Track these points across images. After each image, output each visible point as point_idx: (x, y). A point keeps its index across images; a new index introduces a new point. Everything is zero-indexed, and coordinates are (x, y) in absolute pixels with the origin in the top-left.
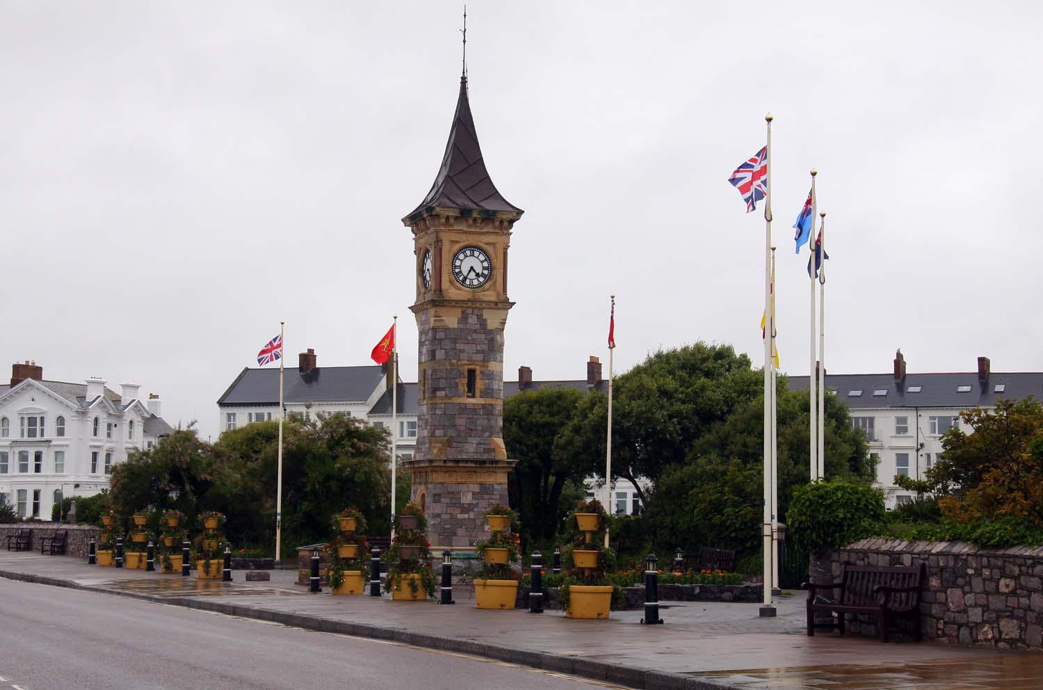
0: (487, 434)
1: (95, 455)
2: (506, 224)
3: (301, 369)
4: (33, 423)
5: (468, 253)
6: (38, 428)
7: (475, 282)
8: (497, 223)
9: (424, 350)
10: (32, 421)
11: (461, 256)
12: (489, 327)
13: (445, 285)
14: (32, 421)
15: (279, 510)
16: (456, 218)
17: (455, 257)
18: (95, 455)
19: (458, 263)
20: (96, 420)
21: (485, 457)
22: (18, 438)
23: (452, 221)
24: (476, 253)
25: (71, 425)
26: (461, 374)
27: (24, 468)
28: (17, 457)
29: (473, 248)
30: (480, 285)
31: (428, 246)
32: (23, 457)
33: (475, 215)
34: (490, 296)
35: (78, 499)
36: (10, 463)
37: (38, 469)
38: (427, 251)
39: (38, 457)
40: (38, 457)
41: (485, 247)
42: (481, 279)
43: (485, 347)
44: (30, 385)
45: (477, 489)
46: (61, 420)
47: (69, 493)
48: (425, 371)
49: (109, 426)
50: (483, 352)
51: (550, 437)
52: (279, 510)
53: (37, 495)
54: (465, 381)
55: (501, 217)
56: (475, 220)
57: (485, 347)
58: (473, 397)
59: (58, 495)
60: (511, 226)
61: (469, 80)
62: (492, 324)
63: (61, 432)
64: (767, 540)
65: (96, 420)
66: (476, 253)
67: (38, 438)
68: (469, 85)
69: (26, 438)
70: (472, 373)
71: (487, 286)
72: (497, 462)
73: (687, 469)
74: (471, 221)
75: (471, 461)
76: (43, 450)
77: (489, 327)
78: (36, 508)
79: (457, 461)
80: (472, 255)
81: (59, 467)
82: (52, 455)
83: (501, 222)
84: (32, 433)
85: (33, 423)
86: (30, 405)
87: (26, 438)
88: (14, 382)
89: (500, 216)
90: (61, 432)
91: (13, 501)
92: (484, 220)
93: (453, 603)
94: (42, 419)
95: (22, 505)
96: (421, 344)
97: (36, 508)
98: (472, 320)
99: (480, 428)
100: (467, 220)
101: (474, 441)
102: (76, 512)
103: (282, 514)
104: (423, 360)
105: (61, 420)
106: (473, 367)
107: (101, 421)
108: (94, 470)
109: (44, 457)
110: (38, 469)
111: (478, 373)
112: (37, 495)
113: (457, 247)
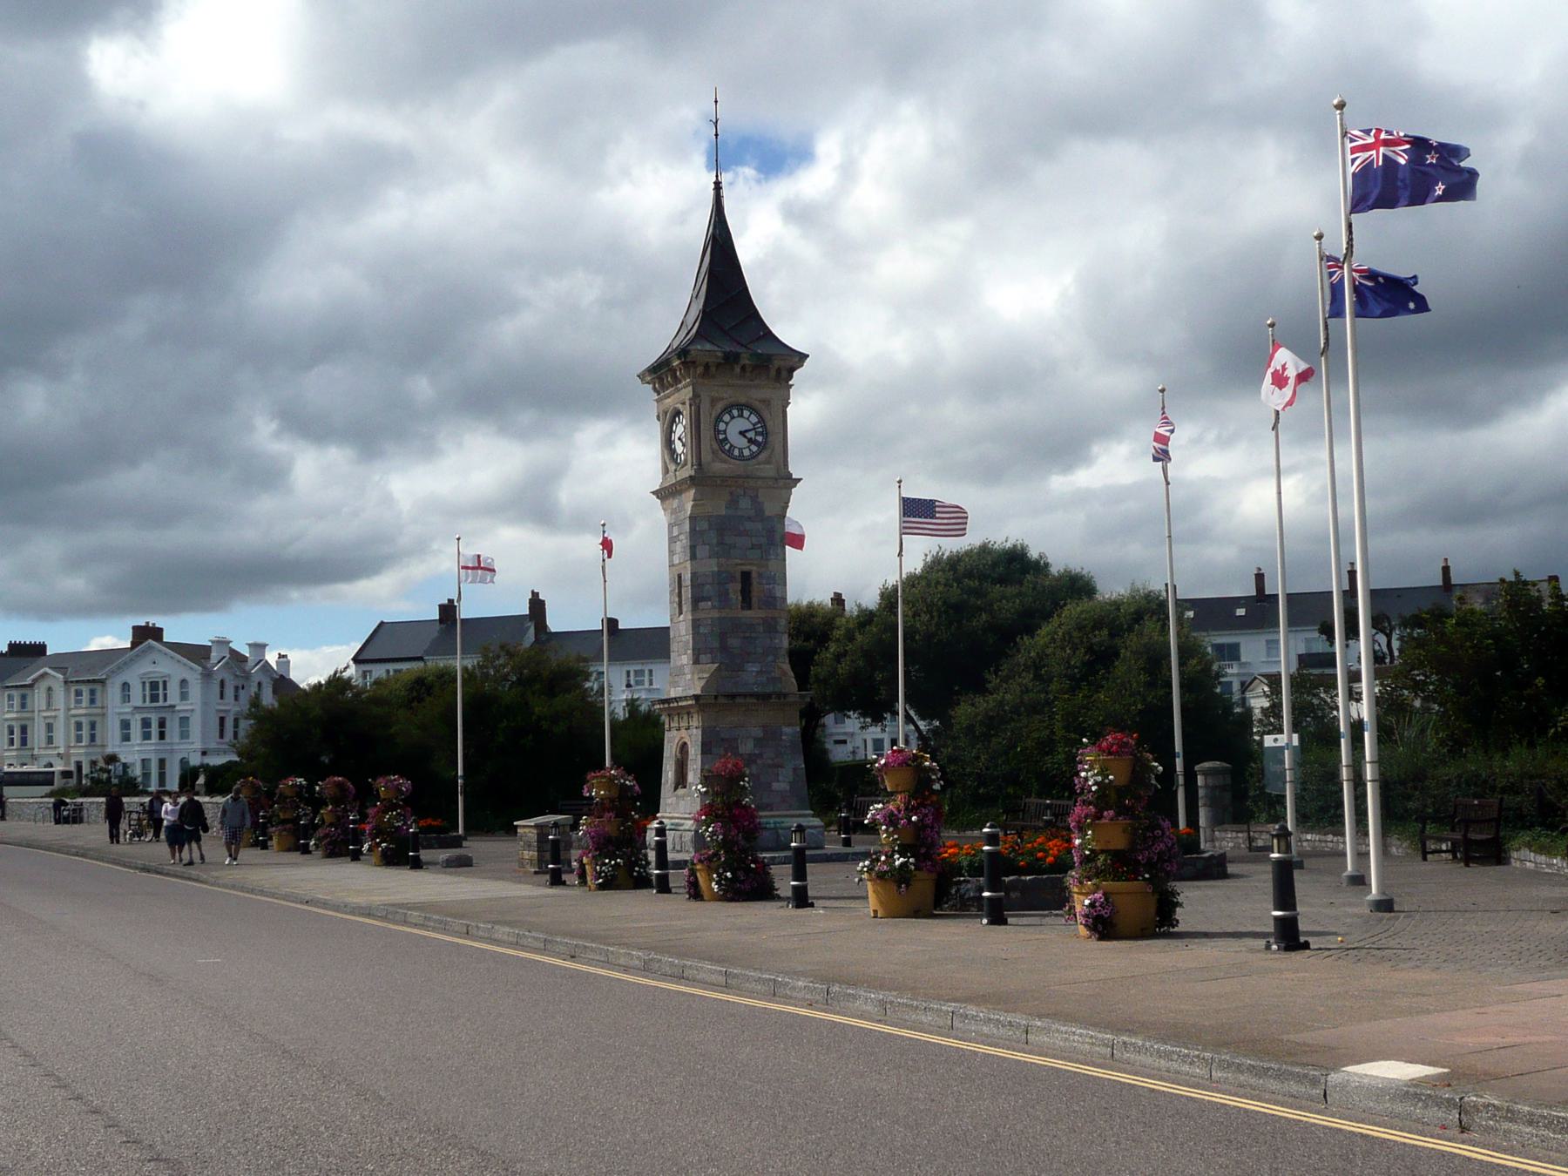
0: (770, 658)
1: (222, 720)
2: (784, 374)
3: (441, 621)
4: (155, 689)
5: (735, 412)
6: (161, 692)
7: (746, 453)
8: (773, 373)
9: (678, 547)
10: (154, 686)
11: (727, 418)
12: (767, 513)
13: (706, 456)
14: (154, 686)
15: (460, 773)
16: (718, 365)
17: (719, 419)
18: (222, 720)
19: (722, 426)
20: (222, 683)
21: (769, 689)
22: (139, 703)
23: (713, 369)
24: (746, 413)
25: (195, 690)
26: (732, 578)
27: (147, 736)
28: (139, 724)
29: (741, 407)
30: (753, 456)
31: (680, 406)
32: (146, 723)
33: (745, 361)
34: (769, 470)
35: (206, 767)
36: (132, 730)
37: (162, 736)
38: (678, 413)
39: (162, 724)
40: (162, 724)
41: (757, 405)
42: (754, 448)
43: (763, 540)
44: (150, 648)
45: (759, 733)
46: (184, 682)
47: (195, 760)
48: (680, 577)
49: (237, 688)
50: (760, 546)
51: (835, 659)
52: (460, 773)
53: (162, 762)
54: (739, 586)
55: (779, 364)
56: (743, 368)
57: (763, 540)
58: (750, 608)
59: (184, 762)
60: (791, 377)
61: (723, 185)
62: (770, 509)
63: (184, 696)
64: (1345, 784)
65: (222, 683)
66: (746, 413)
67: (161, 703)
68: (725, 192)
69: (148, 704)
70: (746, 576)
71: (762, 457)
72: (785, 695)
73: (992, 700)
74: (738, 370)
75: (751, 695)
76: (168, 716)
77: (767, 513)
78: (162, 776)
79: (733, 696)
80: (741, 416)
81: (184, 735)
82: (177, 723)
83: (779, 371)
84: (154, 698)
85: (155, 689)
86: (151, 668)
87: (148, 704)
88: (134, 644)
89: (777, 363)
90: (184, 696)
91: (137, 772)
92: (755, 368)
93: (1306, 946)
94: (165, 683)
95: (146, 775)
96: (672, 540)
97: (162, 776)
98: (745, 504)
99: (760, 650)
100: (733, 369)
101: (753, 668)
102: (1116, 605)
103: (465, 777)
104: (676, 561)
105: (184, 682)
106: (746, 568)
107: (227, 683)
108: (221, 736)
109: (168, 724)
110: (162, 736)
111: (754, 575)
112: (162, 762)
113: (720, 406)
